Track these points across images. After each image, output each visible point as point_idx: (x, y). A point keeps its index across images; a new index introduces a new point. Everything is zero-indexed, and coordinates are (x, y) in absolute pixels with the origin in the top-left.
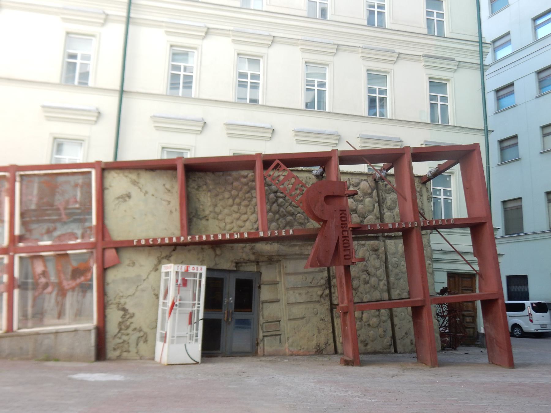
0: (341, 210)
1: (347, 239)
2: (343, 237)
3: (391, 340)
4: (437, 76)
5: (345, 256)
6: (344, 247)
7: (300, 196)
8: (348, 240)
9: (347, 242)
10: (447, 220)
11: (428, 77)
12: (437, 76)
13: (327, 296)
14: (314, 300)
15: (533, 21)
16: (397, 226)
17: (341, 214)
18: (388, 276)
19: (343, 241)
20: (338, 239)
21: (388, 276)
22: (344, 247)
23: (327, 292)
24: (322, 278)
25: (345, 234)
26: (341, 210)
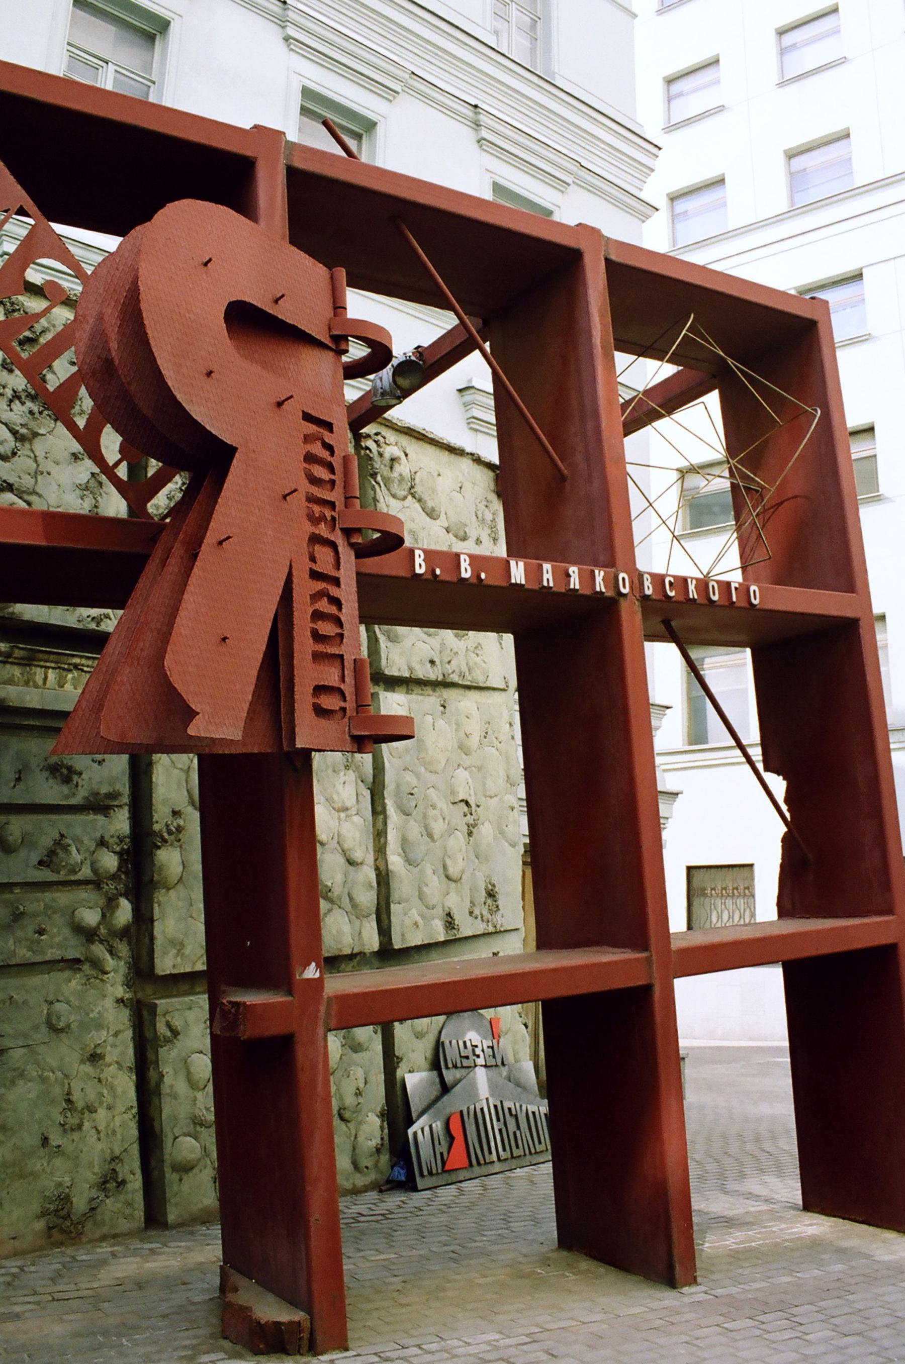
0: (307, 417)
1: (334, 591)
2: (315, 575)
3: (382, 1128)
4: (514, 186)
5: (319, 690)
6: (317, 637)
7: (23, 404)
8: (337, 602)
9: (333, 610)
10: (737, 586)
11: (492, 180)
12: (514, 186)
13: (124, 933)
14: (52, 954)
15: (669, 202)
16: (545, 576)
17: (307, 439)
18: (380, 850)
19: (316, 597)
20: (290, 575)
21: (380, 850)
22: (317, 637)
23: (124, 912)
24: (102, 843)
25: (325, 564)
26: (307, 417)
